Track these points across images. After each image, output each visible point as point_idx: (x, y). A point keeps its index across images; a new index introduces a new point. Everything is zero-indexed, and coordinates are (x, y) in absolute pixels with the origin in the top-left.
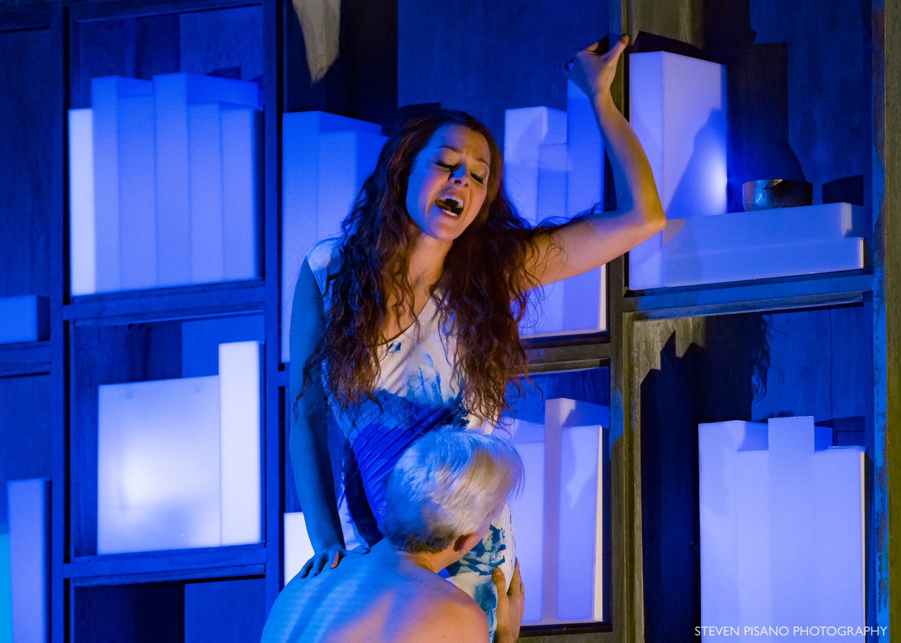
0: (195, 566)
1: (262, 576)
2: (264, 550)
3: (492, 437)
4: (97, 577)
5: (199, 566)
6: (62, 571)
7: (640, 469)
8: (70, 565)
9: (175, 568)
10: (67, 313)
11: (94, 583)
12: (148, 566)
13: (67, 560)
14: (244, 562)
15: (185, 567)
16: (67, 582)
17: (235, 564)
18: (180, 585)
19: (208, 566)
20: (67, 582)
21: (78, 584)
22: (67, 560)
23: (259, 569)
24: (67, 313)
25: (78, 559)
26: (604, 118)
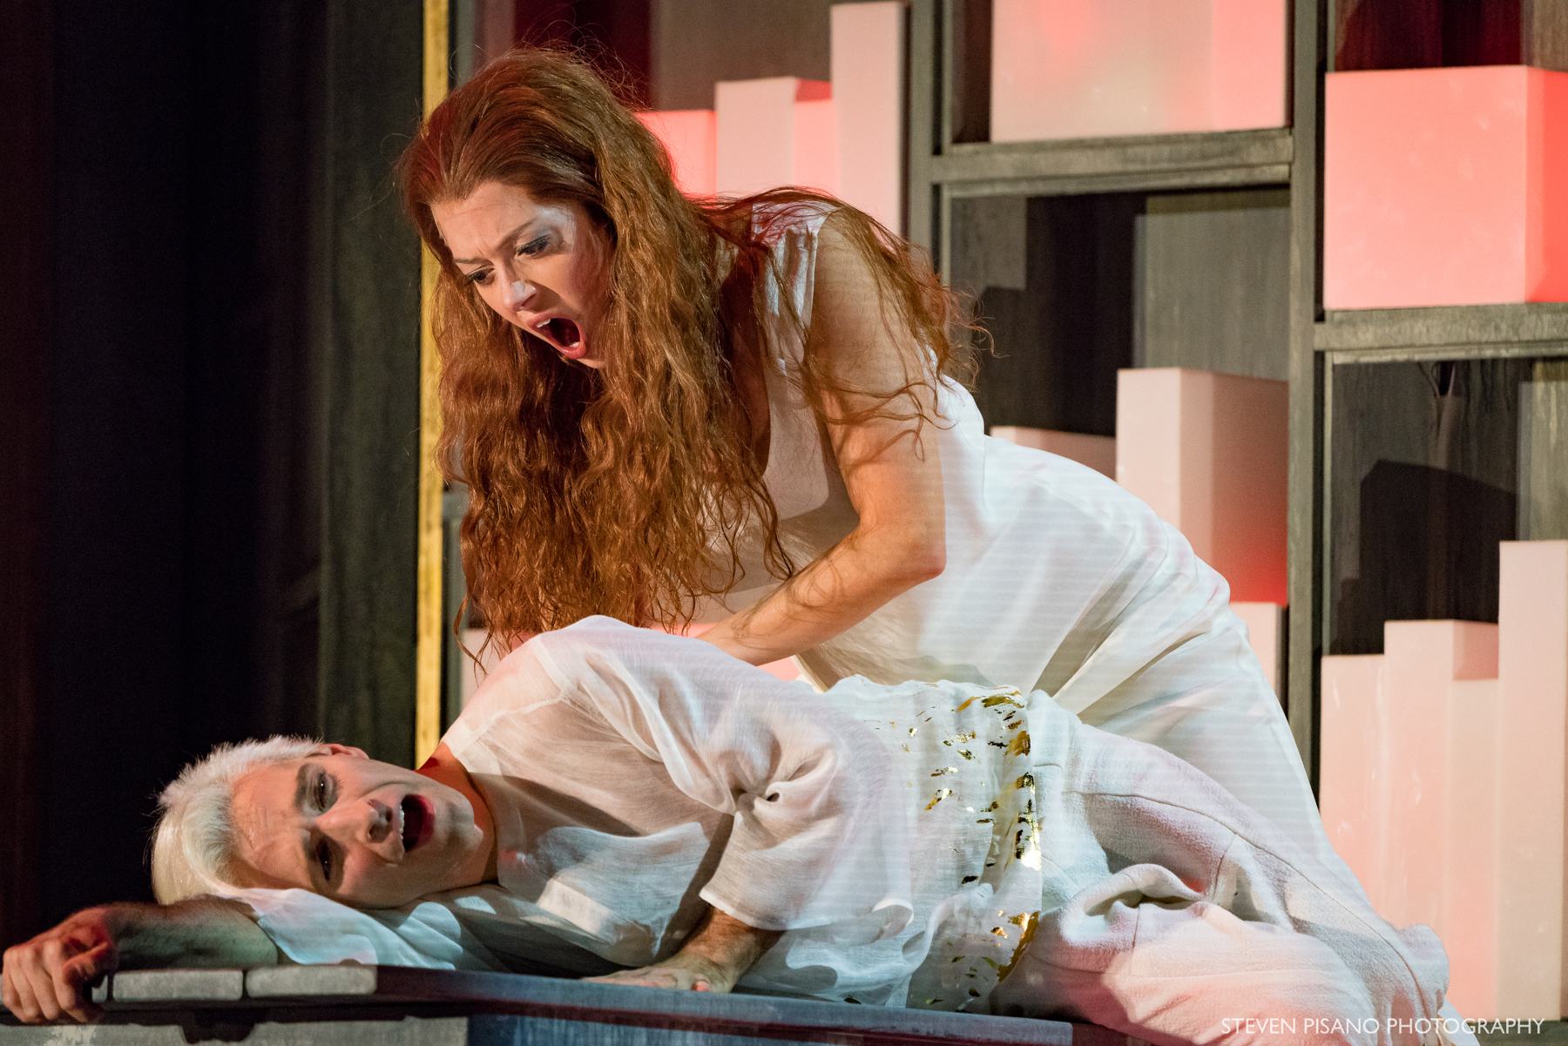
0: (1165, 166)
1: (1284, 186)
2: (1289, 140)
3: (709, 488)
4: (991, 181)
5: (1173, 166)
6: (927, 170)
7: (426, 413)
8: (943, 159)
9: (1132, 167)
10: (1322, 336)
11: (986, 191)
12: (1081, 164)
13: (937, 150)
14: (1254, 160)
15: (1148, 167)
16: (936, 189)
17: (1237, 161)
18: (1132, 203)
19: (1190, 165)
20: (936, 189)
21: (958, 193)
22: (937, 150)
23: (1279, 172)
24: (1322, 336)
25: (957, 149)
26: (1265, 168)
